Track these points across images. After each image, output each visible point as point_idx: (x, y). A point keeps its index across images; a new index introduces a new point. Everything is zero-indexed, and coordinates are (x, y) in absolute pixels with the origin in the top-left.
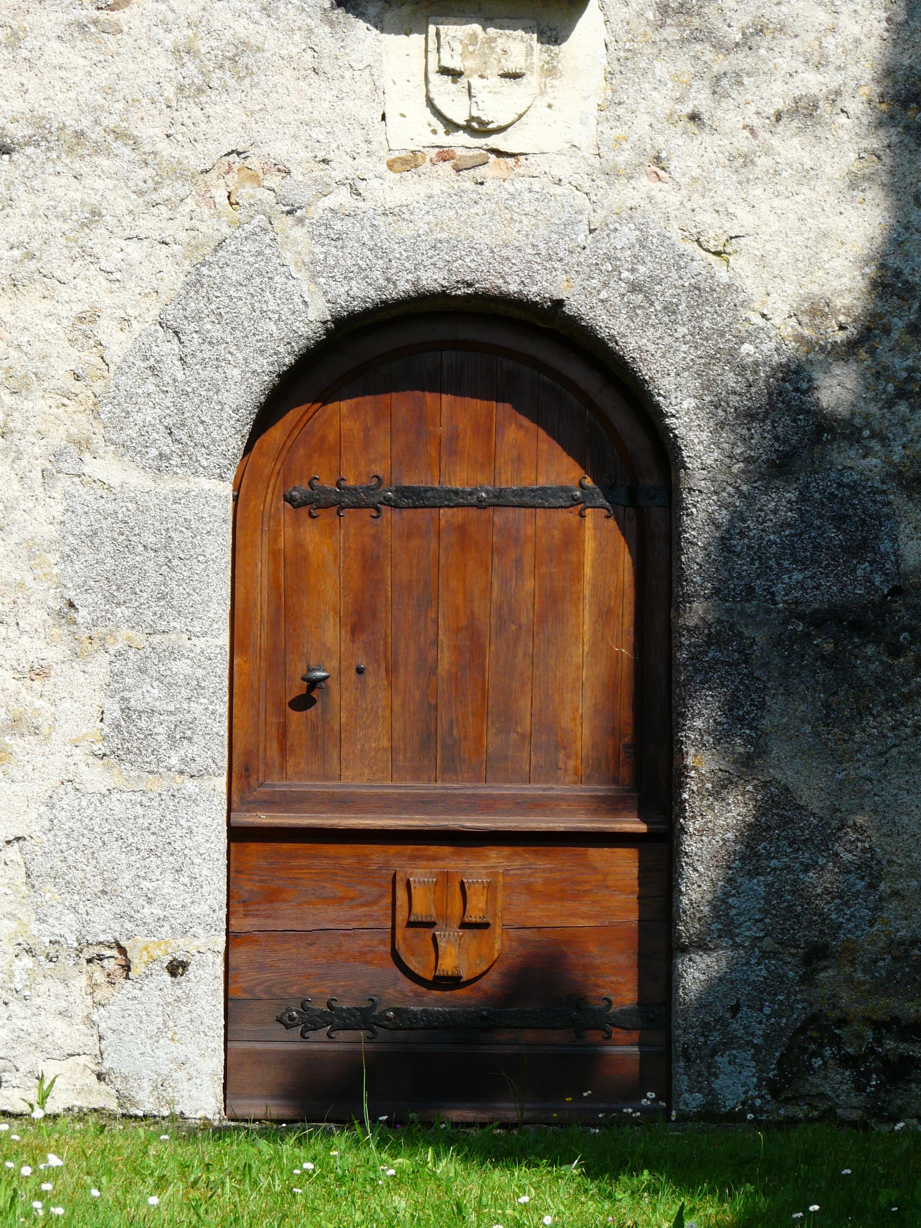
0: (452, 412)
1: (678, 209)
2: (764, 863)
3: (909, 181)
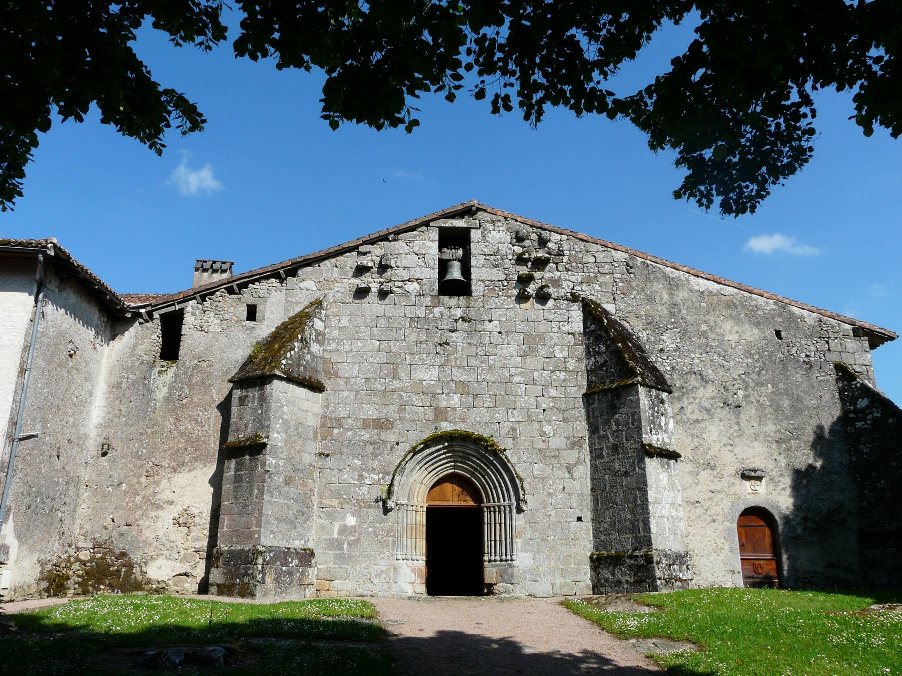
0: (752, 518)
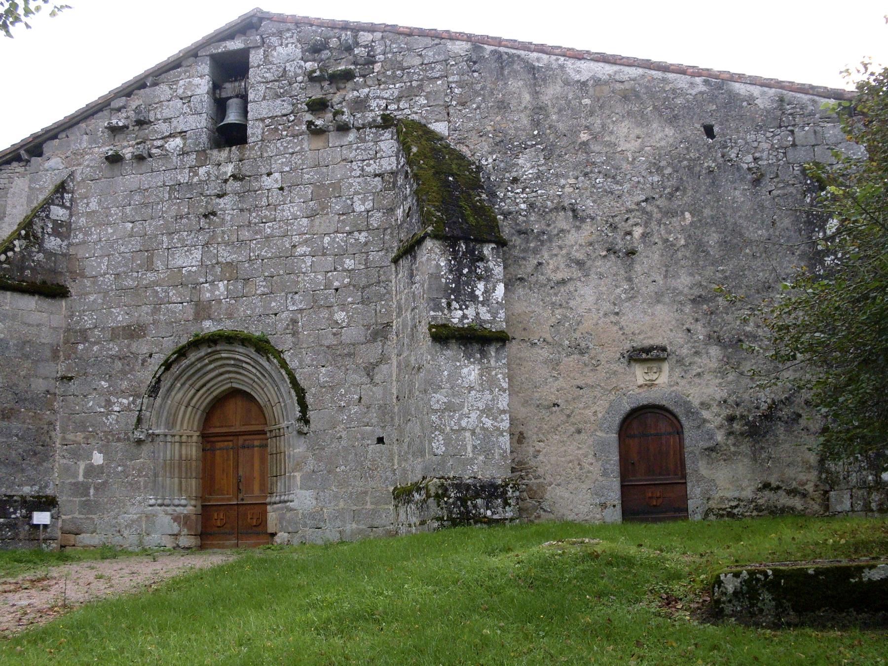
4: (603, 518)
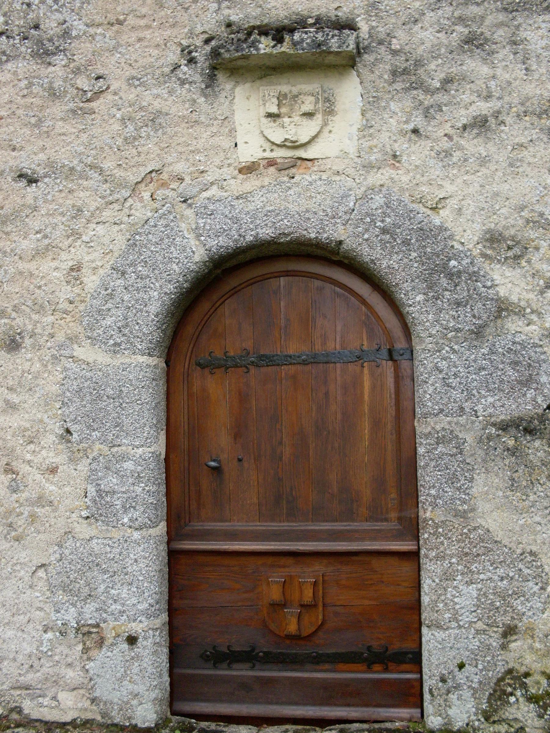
1: (408, 184)
2: (476, 576)
3: (544, 160)
4: (87, 686)
